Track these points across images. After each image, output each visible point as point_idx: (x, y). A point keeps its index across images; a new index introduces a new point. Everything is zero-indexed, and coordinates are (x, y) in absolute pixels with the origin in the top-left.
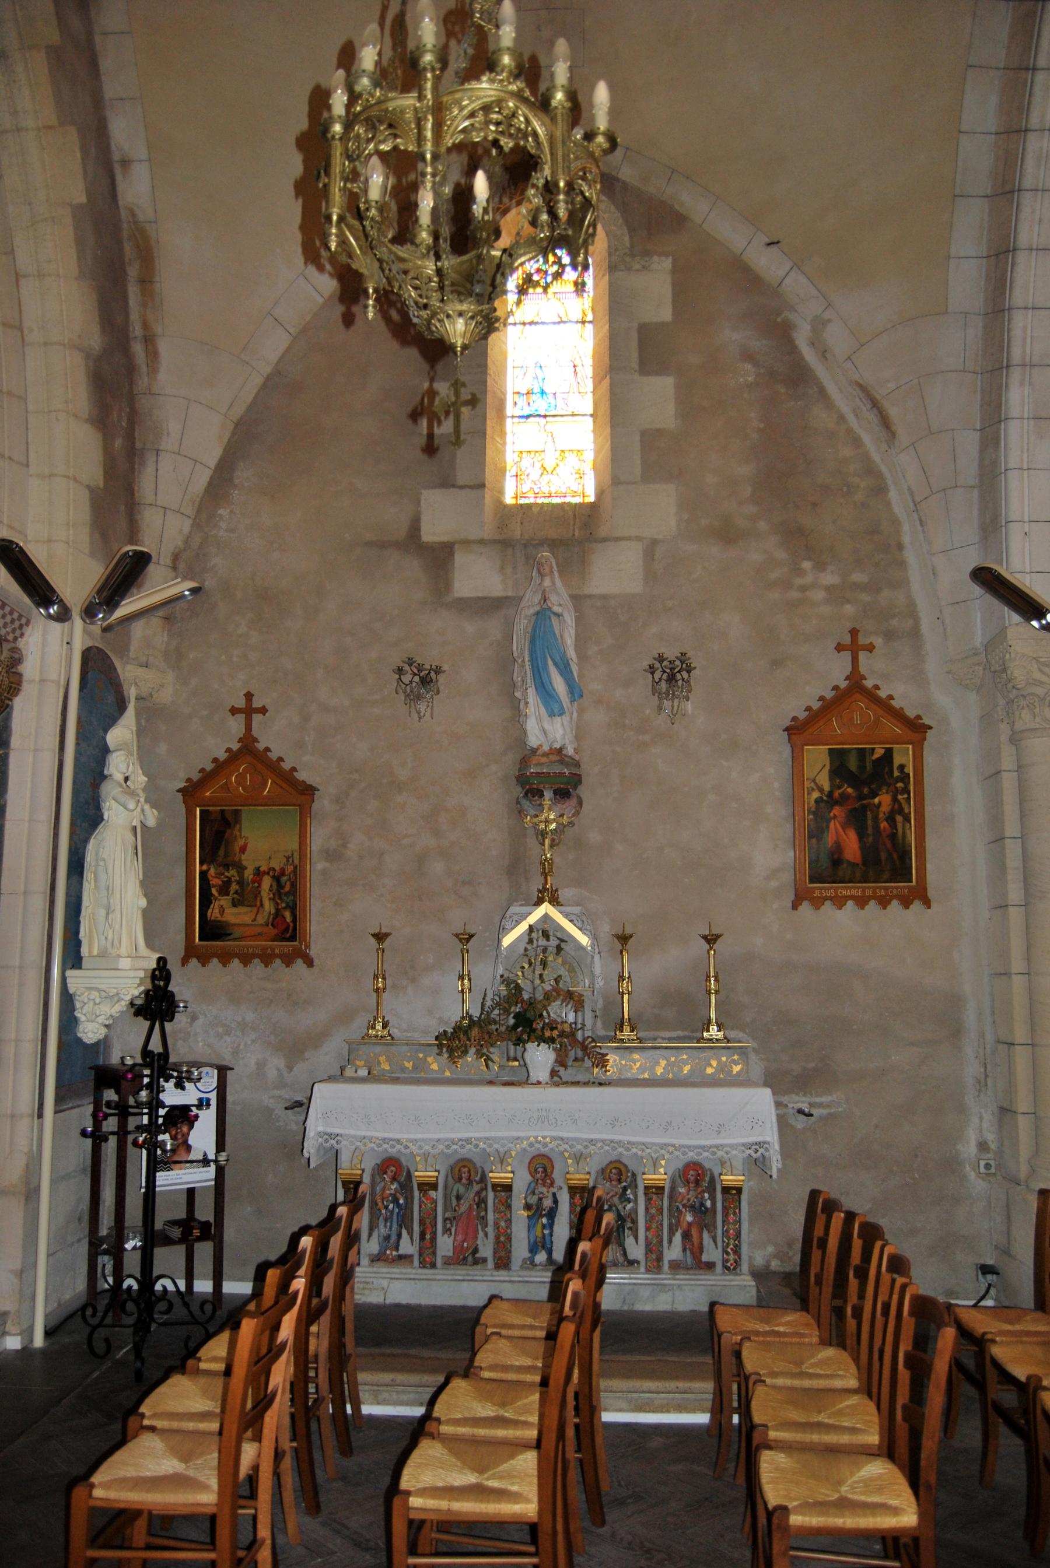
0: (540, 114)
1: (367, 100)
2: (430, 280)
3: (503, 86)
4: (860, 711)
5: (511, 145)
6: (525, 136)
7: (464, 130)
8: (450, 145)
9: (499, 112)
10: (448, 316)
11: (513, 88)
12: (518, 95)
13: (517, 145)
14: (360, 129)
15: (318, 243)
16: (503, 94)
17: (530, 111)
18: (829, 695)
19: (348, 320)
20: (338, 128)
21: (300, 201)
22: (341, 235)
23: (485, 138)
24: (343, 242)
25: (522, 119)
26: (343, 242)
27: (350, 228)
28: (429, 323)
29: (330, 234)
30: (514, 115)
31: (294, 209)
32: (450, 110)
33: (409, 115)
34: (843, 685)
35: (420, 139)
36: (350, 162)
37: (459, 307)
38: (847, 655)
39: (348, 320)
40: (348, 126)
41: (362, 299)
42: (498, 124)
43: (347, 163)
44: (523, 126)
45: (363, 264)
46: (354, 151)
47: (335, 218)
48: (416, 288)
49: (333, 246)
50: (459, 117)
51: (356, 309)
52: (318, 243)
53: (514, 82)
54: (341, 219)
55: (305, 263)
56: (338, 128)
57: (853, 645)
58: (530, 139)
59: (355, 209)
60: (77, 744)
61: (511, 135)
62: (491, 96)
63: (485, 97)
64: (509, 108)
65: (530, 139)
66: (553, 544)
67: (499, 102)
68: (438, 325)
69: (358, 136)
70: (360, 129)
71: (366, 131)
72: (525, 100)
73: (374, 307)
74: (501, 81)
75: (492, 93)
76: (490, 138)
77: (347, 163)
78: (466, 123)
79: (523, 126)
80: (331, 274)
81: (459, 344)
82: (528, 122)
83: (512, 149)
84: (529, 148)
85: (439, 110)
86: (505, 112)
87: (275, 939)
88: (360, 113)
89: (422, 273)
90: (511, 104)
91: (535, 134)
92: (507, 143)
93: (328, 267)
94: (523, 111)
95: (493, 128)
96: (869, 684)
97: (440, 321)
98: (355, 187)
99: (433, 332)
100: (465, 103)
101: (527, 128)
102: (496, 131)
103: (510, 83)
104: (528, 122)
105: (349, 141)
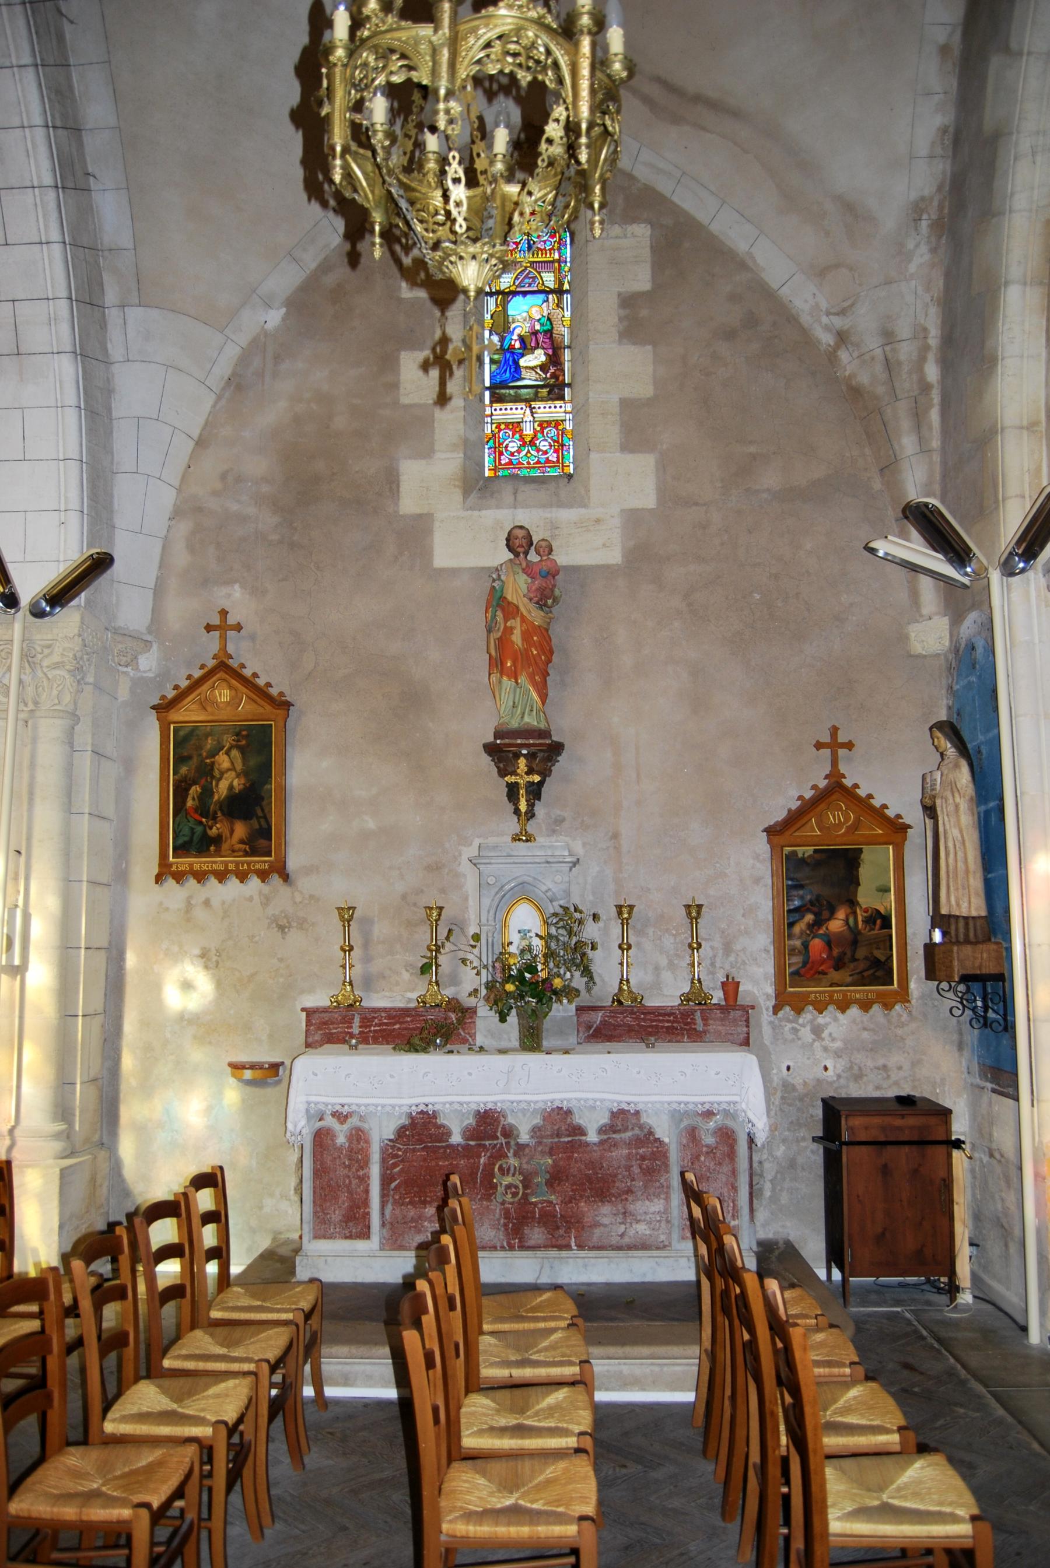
0: (561, 40)
1: (377, 25)
2: (437, 213)
3: (522, 13)
4: (837, 816)
5: (529, 78)
6: (545, 69)
7: (479, 62)
8: (464, 77)
9: (517, 42)
10: (461, 258)
11: (533, 14)
12: (539, 23)
13: (535, 79)
14: (368, 56)
15: (321, 177)
16: (522, 22)
17: (552, 39)
18: (808, 794)
19: (354, 259)
20: (340, 53)
21: (300, 133)
22: (346, 167)
23: (501, 72)
24: (348, 175)
25: (542, 49)
26: (348, 175)
27: (356, 156)
28: (441, 263)
29: (334, 167)
30: (533, 45)
31: (295, 141)
32: (465, 38)
33: (424, 47)
34: (822, 784)
35: (434, 73)
36: (357, 91)
37: (471, 249)
38: (826, 752)
39: (354, 259)
40: (351, 53)
41: (367, 236)
42: (515, 55)
43: (353, 92)
44: (543, 58)
45: (367, 194)
46: (361, 80)
47: (338, 149)
48: (421, 222)
49: (337, 178)
50: (476, 48)
51: (361, 246)
52: (321, 177)
53: (535, 8)
54: (346, 150)
55: (309, 200)
56: (340, 53)
57: (835, 745)
58: (550, 73)
59: (360, 135)
60: (367, 1191)
61: (529, 68)
62: (510, 24)
63: (503, 24)
64: (528, 37)
65: (550, 73)
66: (541, 784)
67: (518, 31)
68: (450, 266)
69: (365, 64)
70: (368, 56)
71: (376, 59)
72: (547, 28)
73: (381, 245)
74: (520, 7)
75: (510, 20)
76: (507, 71)
77: (353, 92)
78: (482, 54)
79: (543, 58)
80: (335, 210)
81: (472, 288)
82: (548, 52)
83: (530, 84)
84: (548, 82)
85: (454, 42)
86: (524, 42)
87: (246, 854)
88: (369, 38)
89: (428, 203)
90: (530, 34)
91: (556, 65)
92: (524, 77)
93: (332, 203)
94: (543, 40)
95: (510, 59)
96: (848, 782)
97: (452, 263)
98: (357, 117)
99: (444, 273)
100: (480, 32)
101: (546, 59)
102: (513, 64)
103: (529, 9)
104: (548, 52)
105: (356, 68)
